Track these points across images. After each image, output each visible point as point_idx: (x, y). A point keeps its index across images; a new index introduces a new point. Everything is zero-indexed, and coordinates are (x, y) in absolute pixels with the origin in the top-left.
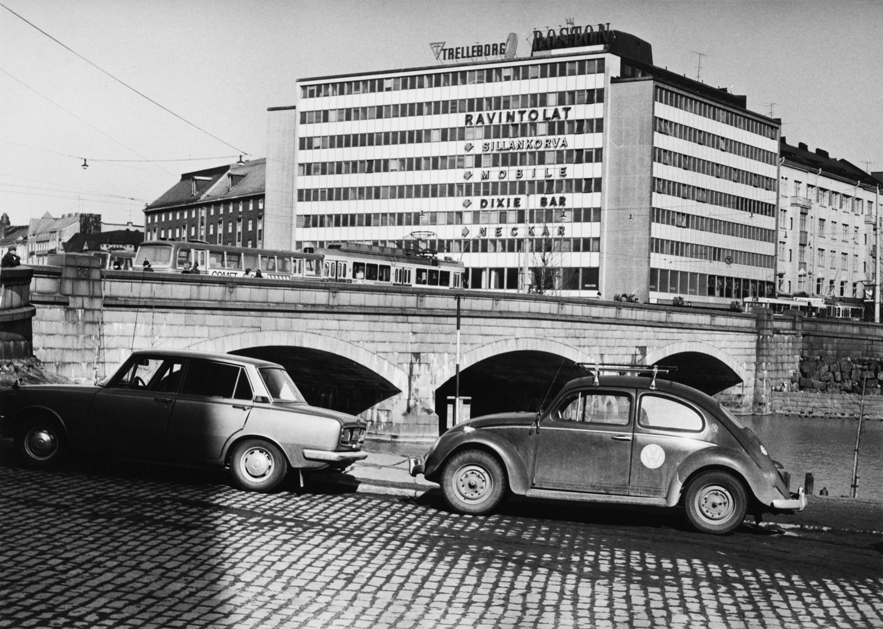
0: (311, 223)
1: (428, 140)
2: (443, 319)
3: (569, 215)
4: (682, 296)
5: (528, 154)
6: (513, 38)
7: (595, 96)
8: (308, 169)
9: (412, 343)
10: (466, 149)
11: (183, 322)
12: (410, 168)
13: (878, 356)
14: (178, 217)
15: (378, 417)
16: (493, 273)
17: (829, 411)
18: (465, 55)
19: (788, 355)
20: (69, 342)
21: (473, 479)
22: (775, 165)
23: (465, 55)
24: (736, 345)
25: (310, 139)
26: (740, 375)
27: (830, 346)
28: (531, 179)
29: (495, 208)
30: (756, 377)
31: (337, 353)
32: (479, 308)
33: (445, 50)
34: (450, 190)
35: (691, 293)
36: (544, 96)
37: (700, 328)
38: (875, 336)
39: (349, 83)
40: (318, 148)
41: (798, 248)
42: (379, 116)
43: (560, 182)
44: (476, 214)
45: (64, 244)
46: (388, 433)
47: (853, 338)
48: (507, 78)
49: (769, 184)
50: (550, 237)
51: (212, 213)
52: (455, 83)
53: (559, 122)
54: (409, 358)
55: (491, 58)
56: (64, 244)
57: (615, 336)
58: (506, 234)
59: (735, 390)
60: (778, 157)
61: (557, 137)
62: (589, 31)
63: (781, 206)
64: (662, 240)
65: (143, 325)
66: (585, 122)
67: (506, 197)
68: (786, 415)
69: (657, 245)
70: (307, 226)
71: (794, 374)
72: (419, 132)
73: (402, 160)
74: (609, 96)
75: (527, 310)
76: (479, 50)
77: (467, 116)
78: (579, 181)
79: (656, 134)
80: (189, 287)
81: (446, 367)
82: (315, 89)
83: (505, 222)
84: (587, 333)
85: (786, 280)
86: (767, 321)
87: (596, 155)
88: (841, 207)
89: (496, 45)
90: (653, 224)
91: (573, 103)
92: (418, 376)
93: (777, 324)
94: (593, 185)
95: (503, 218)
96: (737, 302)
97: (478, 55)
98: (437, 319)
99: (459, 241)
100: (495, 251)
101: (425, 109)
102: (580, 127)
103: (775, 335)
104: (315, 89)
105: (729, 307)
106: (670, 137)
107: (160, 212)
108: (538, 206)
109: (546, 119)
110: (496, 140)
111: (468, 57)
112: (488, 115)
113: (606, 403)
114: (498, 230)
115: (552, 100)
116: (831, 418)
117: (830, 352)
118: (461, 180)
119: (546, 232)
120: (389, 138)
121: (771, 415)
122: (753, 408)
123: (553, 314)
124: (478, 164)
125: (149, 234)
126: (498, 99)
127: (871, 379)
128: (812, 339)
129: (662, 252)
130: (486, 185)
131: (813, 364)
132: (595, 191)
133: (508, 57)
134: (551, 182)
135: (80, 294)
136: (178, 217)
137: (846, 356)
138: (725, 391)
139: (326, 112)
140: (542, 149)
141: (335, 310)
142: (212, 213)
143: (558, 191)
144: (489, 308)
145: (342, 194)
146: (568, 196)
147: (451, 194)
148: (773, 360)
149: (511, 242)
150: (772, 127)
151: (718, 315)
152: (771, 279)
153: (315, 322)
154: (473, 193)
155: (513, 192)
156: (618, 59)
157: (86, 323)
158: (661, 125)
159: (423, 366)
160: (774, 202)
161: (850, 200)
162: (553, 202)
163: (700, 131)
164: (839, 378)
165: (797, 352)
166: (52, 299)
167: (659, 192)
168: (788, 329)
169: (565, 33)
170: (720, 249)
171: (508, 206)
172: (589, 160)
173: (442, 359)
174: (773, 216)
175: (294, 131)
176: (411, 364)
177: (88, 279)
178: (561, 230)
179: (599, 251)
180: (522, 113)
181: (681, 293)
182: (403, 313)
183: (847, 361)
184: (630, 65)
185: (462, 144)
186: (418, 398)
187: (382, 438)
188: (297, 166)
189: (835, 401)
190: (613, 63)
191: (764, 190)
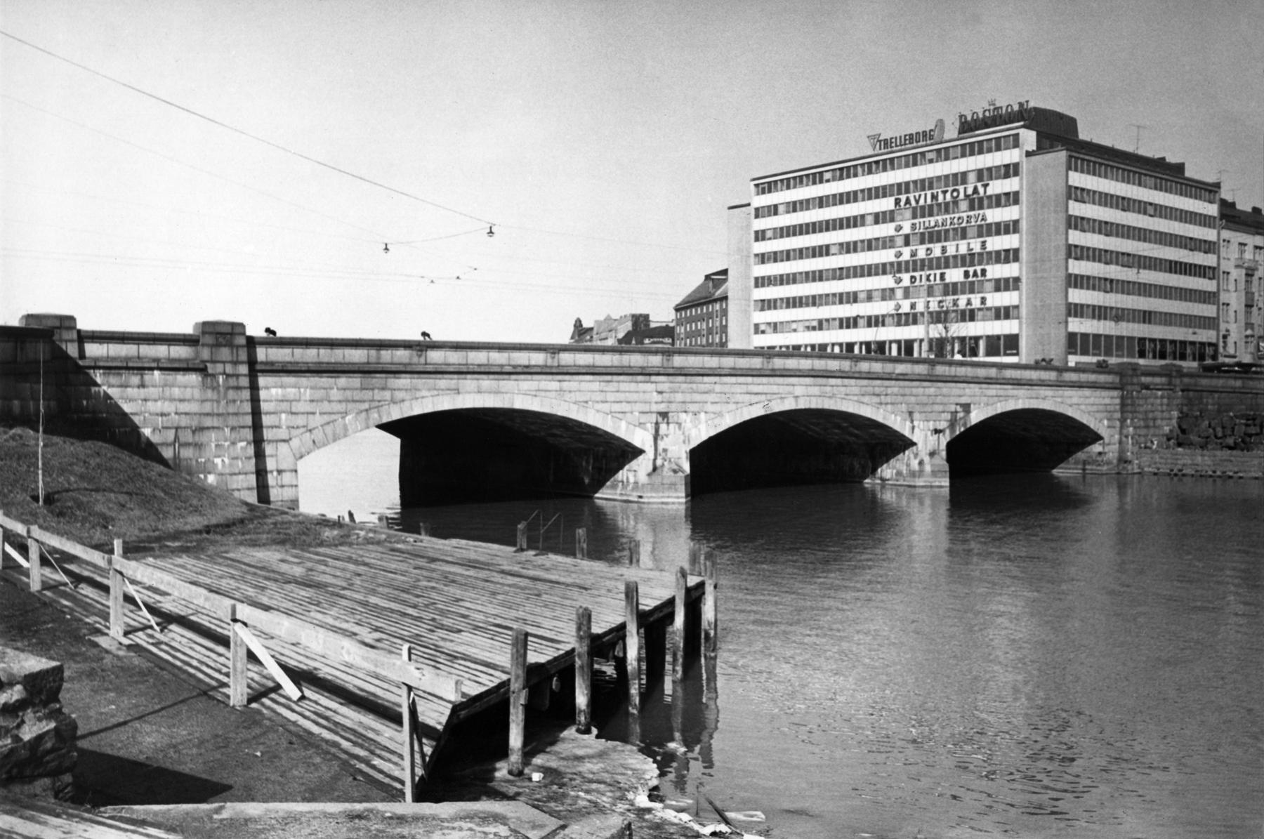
1: (863, 224)
3: (989, 286)
4: (1106, 358)
6: (940, 124)
7: (1010, 170)
8: (763, 258)
9: (656, 403)
11: (358, 385)
12: (848, 252)
15: (628, 478)
17: (1199, 468)
19: (1162, 411)
20: (207, 407)
22: (1214, 228)
24: (1092, 400)
25: (764, 231)
26: (1099, 432)
27: (1210, 401)
28: (954, 253)
30: (1121, 433)
31: (560, 413)
33: (880, 141)
34: (882, 269)
36: (964, 174)
40: (770, 239)
43: (980, 254)
44: (906, 290)
46: (636, 494)
47: (1234, 392)
48: (931, 161)
49: (1208, 247)
50: (973, 307)
52: (885, 170)
58: (934, 306)
59: (1097, 448)
60: (1217, 220)
61: (976, 212)
63: (1223, 268)
65: (308, 390)
67: (932, 272)
69: (1076, 310)
70: (762, 309)
71: (1171, 431)
73: (841, 245)
74: (1024, 168)
75: (810, 367)
76: (911, 138)
77: (896, 199)
78: (998, 253)
79: (1071, 203)
80: (366, 352)
81: (703, 427)
82: (765, 187)
83: (933, 296)
84: (915, 391)
85: (1230, 341)
86: (1132, 376)
91: (991, 179)
92: (667, 436)
98: (689, 378)
99: (892, 315)
101: (860, 195)
106: (1088, 205)
107: (685, 308)
109: (967, 196)
110: (922, 220)
111: (901, 145)
115: (972, 177)
116: (1201, 476)
117: (1210, 407)
118: (893, 259)
119: (969, 303)
120: (828, 226)
121: (1140, 473)
122: (1118, 465)
123: (843, 372)
126: (923, 181)
128: (1191, 394)
130: (915, 262)
137: (1227, 411)
138: (1086, 450)
139: (776, 206)
140: (964, 225)
143: (980, 264)
144: (758, 366)
146: (989, 268)
148: (1141, 416)
149: (938, 313)
150: (1210, 191)
152: (1214, 341)
153: (527, 384)
155: (939, 268)
157: (228, 388)
159: (671, 426)
160: (1215, 265)
162: (975, 274)
164: (1220, 434)
167: (1076, 259)
176: (657, 423)
178: (983, 300)
180: (945, 192)
182: (645, 373)
185: (892, 226)
187: (631, 498)
189: (1206, 458)
190: (1029, 138)
191: (1202, 254)
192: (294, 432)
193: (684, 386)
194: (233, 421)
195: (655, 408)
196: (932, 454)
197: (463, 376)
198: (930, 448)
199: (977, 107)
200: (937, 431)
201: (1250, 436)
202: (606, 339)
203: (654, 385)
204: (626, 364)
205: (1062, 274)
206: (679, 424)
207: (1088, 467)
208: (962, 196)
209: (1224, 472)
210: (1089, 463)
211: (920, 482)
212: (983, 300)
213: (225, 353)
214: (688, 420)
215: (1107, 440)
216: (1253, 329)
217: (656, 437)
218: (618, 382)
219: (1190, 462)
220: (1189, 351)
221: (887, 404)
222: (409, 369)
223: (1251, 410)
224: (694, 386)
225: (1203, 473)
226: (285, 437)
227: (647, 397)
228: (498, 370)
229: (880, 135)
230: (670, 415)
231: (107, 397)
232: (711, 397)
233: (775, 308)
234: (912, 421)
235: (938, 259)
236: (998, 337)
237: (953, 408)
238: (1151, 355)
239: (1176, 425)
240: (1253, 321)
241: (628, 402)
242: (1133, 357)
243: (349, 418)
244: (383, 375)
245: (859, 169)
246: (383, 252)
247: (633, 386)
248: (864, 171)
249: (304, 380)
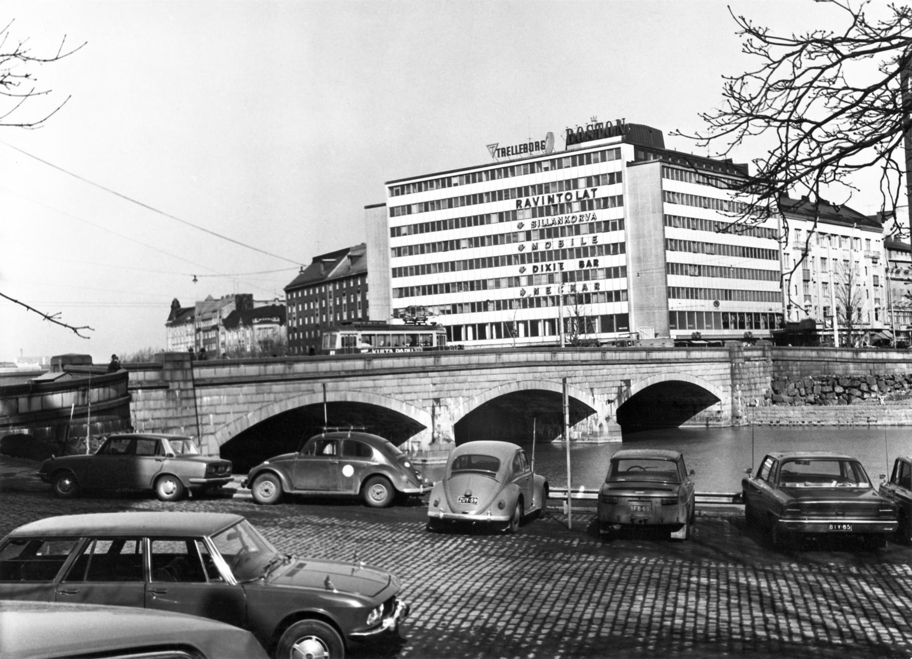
0: (404, 294)
1: (489, 222)
2: (457, 373)
3: (601, 274)
4: (699, 331)
5: (566, 228)
6: (550, 136)
7: (615, 178)
8: (399, 252)
9: (432, 392)
10: (518, 227)
12: (477, 245)
13: (834, 374)
14: (311, 293)
15: (412, 448)
16: (547, 323)
17: (792, 420)
18: (514, 152)
19: (760, 377)
20: (170, 413)
21: (267, 487)
23: (514, 152)
24: (712, 372)
25: (399, 228)
26: (717, 396)
27: (794, 368)
29: (544, 272)
30: (732, 396)
32: (485, 361)
33: (498, 150)
34: (509, 260)
35: (707, 328)
36: (576, 181)
37: (677, 361)
38: (830, 358)
39: (425, 182)
40: (405, 234)
41: (802, 283)
42: (450, 206)
43: (592, 247)
45: (224, 320)
46: (419, 459)
47: (812, 361)
48: (546, 169)
50: (588, 291)
51: (337, 287)
52: (506, 176)
53: (589, 201)
54: (431, 403)
55: (535, 153)
56: (224, 320)
57: (602, 374)
59: (715, 408)
61: (587, 212)
62: (609, 126)
64: (678, 288)
66: (609, 199)
67: (552, 263)
68: (760, 425)
69: (673, 292)
70: (401, 296)
71: (767, 392)
72: (482, 216)
73: (470, 240)
74: (626, 177)
75: (525, 360)
76: (525, 148)
77: (517, 201)
78: (608, 246)
79: (666, 204)
81: (461, 407)
82: (398, 189)
83: (553, 282)
84: (594, 372)
86: (738, 351)
87: (619, 225)
88: (840, 246)
89: (538, 142)
90: (669, 276)
91: (599, 185)
92: (440, 415)
93: (746, 354)
94: (619, 248)
95: (551, 279)
96: (750, 333)
97: (525, 152)
98: (452, 373)
99: (518, 300)
100: (547, 306)
101: (485, 198)
102: (605, 203)
103: (747, 363)
104: (398, 189)
105: (743, 337)
107: (297, 290)
108: (578, 268)
109: (578, 199)
110: (541, 219)
111: (517, 153)
112: (534, 199)
113: (598, 425)
114: (548, 289)
115: (582, 183)
116: (794, 425)
117: (795, 373)
118: (517, 252)
119: (585, 288)
122: (732, 420)
124: (528, 238)
125: (290, 308)
126: (540, 186)
127: (830, 392)
128: (780, 363)
129: (679, 297)
131: (782, 383)
132: (621, 253)
133: (548, 152)
134: (586, 249)
135: (177, 379)
136: (311, 293)
140: (577, 223)
141: (371, 373)
142: (337, 287)
143: (593, 255)
145: (425, 269)
147: (510, 263)
148: (746, 382)
151: (693, 350)
152: (780, 311)
153: (355, 383)
154: (526, 261)
155: (557, 258)
156: (632, 147)
157: (182, 399)
158: (667, 196)
159: (442, 408)
161: (848, 240)
162: (589, 264)
163: (705, 198)
164: (803, 393)
165: (768, 374)
166: (156, 385)
167: (672, 250)
168: (759, 357)
169: (590, 128)
170: (730, 291)
171: (554, 269)
172: (614, 229)
173: (458, 402)
174: (777, 259)
175: (385, 223)
176: (433, 407)
177: (182, 369)
178: (597, 286)
179: (627, 300)
180: (559, 196)
181: (698, 328)
182: (424, 370)
183: (809, 379)
184: (642, 150)
185: (516, 223)
186: (440, 431)
187: (416, 462)
188: (390, 250)
189: (796, 412)
190: (628, 151)
193: (449, 378)
195: (432, 395)
196: (608, 419)
197: (316, 381)
198: (605, 415)
199: (582, 122)
200: (610, 402)
201: (826, 393)
202: (210, 319)
203: (430, 379)
204: (412, 365)
205: (661, 264)
206: (446, 406)
207: (709, 423)
208: (574, 199)
209: (810, 422)
210: (711, 420)
211: (601, 440)
212: (597, 286)
214: (452, 403)
215: (723, 401)
216: (810, 300)
217: (433, 416)
218: (409, 378)
219: (785, 415)
220: (762, 321)
221: (576, 383)
222: (284, 377)
223: (825, 374)
224: (455, 378)
225: (795, 423)
226: (212, 431)
227: (427, 388)
228: (337, 374)
229: (497, 144)
230: (441, 400)
232: (466, 386)
233: (412, 295)
234: (593, 395)
235: (556, 251)
236: (611, 316)
237: (619, 384)
238: (733, 326)
239: (770, 387)
240: (810, 294)
241: (415, 393)
242: (720, 328)
243: (250, 415)
244: (269, 383)
245: (484, 175)
246: (193, 283)
247: (418, 381)
248: (487, 177)
249: (223, 390)
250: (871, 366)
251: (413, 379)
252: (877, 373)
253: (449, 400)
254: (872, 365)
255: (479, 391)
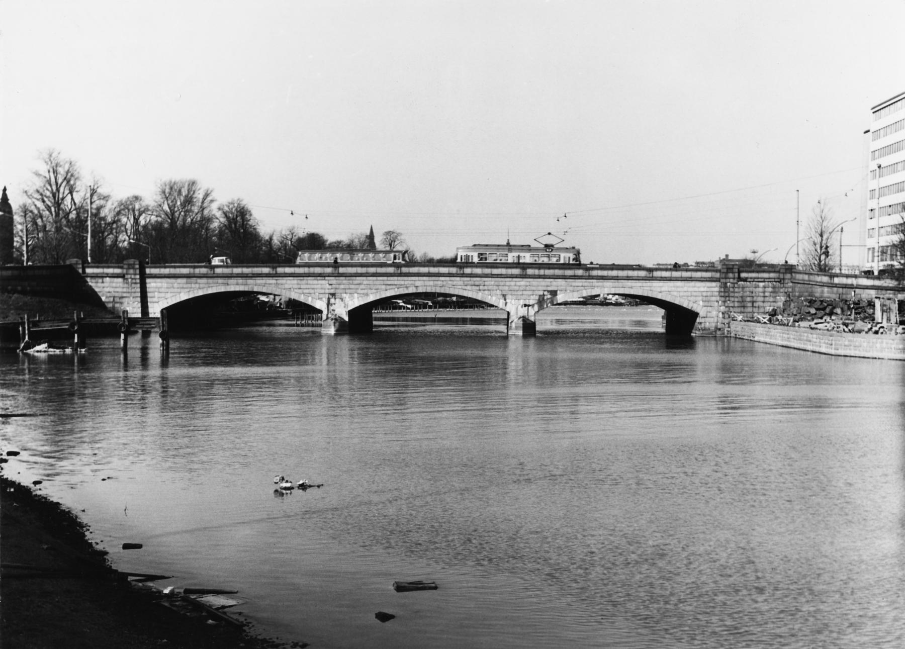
2: (354, 278)
20: (125, 290)
153: (260, 281)
157: (132, 283)
159: (337, 300)
192: (160, 299)
194: (134, 295)
195: (327, 291)
206: (342, 299)
213: (131, 271)
217: (329, 304)
224: (351, 282)
227: (323, 286)
231: (91, 286)
234: (505, 300)
247: (315, 282)
250: (840, 290)
251: (311, 281)
252: (844, 297)
253: (344, 295)
254: (841, 289)
255: (374, 291)
